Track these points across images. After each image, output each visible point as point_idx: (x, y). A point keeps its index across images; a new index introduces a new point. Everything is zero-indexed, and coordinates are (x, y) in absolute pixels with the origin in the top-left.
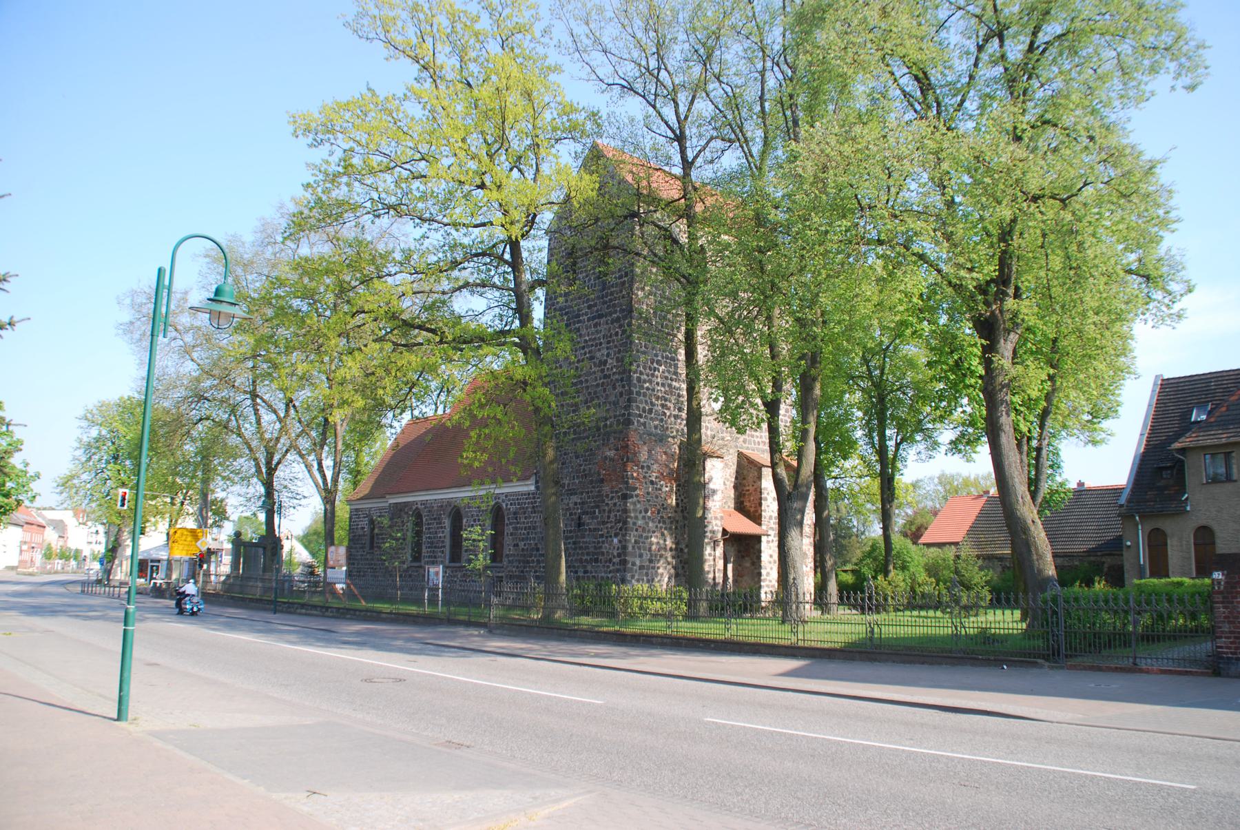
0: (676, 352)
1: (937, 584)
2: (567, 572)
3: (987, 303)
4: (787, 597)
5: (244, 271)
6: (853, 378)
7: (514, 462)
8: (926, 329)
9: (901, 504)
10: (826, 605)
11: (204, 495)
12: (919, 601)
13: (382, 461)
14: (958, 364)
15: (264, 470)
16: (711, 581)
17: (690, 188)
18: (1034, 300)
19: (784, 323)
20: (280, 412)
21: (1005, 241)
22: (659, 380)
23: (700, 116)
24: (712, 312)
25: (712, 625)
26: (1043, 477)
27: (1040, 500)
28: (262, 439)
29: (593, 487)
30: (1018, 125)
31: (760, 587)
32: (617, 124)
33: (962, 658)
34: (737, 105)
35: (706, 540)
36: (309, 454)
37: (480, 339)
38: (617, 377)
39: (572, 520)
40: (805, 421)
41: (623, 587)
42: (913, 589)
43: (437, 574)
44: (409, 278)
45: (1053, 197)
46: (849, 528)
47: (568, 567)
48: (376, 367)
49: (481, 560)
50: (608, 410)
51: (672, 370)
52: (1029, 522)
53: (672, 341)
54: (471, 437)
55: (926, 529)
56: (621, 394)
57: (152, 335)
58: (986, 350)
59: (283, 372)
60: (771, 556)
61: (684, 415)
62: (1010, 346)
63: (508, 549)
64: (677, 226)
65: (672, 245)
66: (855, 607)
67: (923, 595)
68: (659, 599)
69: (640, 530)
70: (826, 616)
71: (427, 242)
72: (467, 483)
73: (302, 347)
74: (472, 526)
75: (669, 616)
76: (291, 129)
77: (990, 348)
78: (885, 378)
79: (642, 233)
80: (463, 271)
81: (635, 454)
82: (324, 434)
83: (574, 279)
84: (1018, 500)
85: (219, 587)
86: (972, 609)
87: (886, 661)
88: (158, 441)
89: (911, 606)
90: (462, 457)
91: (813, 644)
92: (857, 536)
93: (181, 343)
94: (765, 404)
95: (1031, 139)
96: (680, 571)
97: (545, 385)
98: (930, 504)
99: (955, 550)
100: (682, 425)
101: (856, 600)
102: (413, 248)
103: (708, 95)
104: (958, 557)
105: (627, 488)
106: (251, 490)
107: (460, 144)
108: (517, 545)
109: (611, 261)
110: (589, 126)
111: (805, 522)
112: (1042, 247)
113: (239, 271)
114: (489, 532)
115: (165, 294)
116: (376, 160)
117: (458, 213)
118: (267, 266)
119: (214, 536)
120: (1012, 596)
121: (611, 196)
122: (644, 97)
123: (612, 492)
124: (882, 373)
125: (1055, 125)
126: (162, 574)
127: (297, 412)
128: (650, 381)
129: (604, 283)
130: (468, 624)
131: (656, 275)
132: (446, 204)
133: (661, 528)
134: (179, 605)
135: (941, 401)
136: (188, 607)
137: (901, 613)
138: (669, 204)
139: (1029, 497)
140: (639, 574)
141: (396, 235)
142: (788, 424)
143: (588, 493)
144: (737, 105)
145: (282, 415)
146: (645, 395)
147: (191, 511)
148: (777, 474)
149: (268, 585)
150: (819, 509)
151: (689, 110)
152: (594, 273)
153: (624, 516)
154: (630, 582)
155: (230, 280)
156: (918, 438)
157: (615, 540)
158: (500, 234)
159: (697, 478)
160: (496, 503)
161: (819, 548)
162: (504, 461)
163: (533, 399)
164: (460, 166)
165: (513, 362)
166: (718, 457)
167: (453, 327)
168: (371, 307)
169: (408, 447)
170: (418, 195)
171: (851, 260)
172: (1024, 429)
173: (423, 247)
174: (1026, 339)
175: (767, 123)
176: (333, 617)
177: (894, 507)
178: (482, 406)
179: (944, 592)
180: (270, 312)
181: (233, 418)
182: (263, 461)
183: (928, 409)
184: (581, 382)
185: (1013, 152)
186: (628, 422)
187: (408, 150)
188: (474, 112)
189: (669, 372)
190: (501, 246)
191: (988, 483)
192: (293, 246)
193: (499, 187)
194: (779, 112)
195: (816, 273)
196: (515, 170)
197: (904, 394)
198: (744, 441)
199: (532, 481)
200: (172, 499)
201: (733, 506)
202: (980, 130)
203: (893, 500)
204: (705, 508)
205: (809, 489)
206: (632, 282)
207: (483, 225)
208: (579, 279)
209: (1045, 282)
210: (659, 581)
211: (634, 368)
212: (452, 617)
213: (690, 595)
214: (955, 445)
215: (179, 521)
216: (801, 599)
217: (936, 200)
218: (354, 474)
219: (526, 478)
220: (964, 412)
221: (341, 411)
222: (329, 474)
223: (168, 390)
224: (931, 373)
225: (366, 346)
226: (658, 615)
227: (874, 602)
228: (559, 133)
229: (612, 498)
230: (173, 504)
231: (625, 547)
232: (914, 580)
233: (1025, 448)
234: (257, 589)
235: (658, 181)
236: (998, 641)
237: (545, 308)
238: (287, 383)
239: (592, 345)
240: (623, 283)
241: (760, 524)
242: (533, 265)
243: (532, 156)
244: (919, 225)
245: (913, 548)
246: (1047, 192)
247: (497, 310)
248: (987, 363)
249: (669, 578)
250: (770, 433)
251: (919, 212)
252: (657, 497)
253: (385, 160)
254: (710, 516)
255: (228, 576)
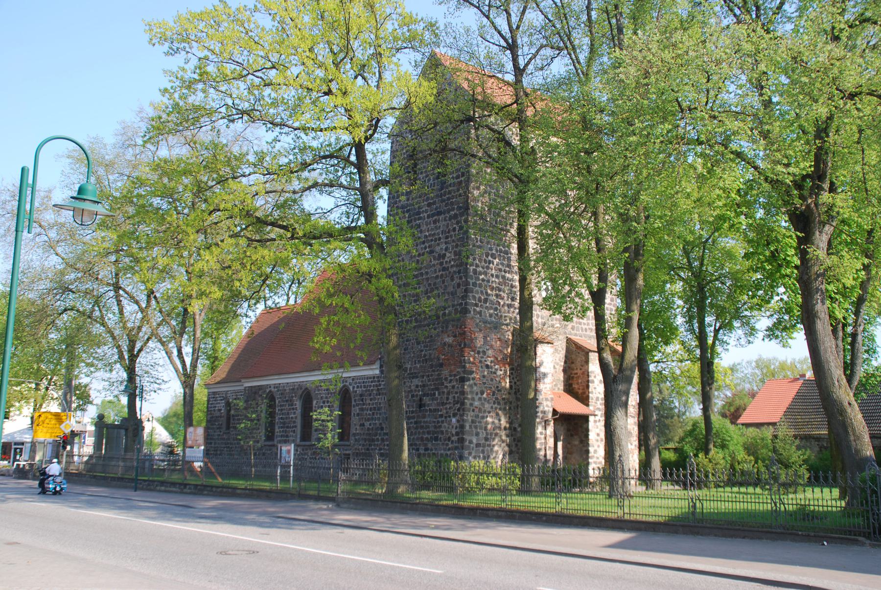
0: (509, 246)
1: (756, 462)
2: (409, 450)
3: (802, 197)
6: (673, 269)
7: (361, 348)
9: (720, 386)
10: (650, 480)
11: (69, 384)
12: (738, 478)
13: (238, 348)
14: (774, 256)
16: (542, 458)
17: (522, 93)
18: (849, 193)
19: (608, 219)
20: (141, 303)
21: (821, 138)
22: (493, 271)
23: (531, 26)
24: (541, 209)
25: (543, 499)
26: (859, 361)
27: (856, 383)
28: (124, 327)
29: (434, 371)
30: (836, 25)
31: (588, 464)
32: (453, 34)
33: (782, 533)
34: (565, 15)
35: (538, 420)
36: (169, 342)
37: (329, 234)
38: (455, 269)
39: (414, 401)
40: (629, 309)
42: (732, 467)
43: (288, 452)
45: (871, 93)
46: (672, 409)
47: (410, 445)
48: (232, 261)
49: (330, 439)
50: (446, 300)
51: (506, 262)
52: (846, 404)
53: (505, 235)
54: (321, 324)
55: (745, 410)
56: (459, 285)
57: (17, 231)
60: (598, 435)
62: (825, 238)
63: (355, 428)
64: (510, 129)
65: (505, 147)
66: (677, 483)
67: (743, 472)
68: (494, 475)
69: (477, 410)
70: (650, 491)
71: (278, 146)
73: (163, 243)
74: (322, 407)
75: (504, 491)
76: (147, 37)
77: (805, 241)
78: (704, 268)
79: (477, 137)
80: (312, 172)
81: (472, 340)
82: (183, 322)
83: (415, 179)
84: (834, 384)
85: (82, 467)
87: (708, 534)
88: (23, 331)
89: (731, 483)
90: (313, 342)
91: (639, 518)
92: (679, 417)
93: (46, 238)
94: (592, 293)
95: (849, 38)
96: (514, 449)
97: (389, 277)
98: (747, 386)
100: (515, 314)
101: (678, 476)
102: (265, 151)
103: (538, 6)
104: (776, 437)
105: (464, 372)
107: (308, 53)
108: (363, 425)
110: (427, 35)
111: (630, 403)
112: (858, 143)
113: (101, 172)
114: (336, 413)
115: (29, 192)
116: (229, 68)
117: (306, 118)
119: (77, 419)
120: (830, 475)
122: (478, 8)
123: (451, 376)
124: (702, 264)
125: (875, 23)
126: (25, 456)
127: (158, 302)
128: (486, 274)
130: (318, 498)
133: (496, 408)
134: (42, 485)
135: (758, 290)
136: (51, 486)
137: (722, 489)
138: (502, 109)
139: (845, 380)
140: (476, 451)
141: (250, 138)
142: (613, 312)
144: (565, 15)
145: (144, 306)
146: (480, 286)
147: (56, 396)
149: (128, 464)
151: (521, 20)
153: (462, 397)
154: (467, 459)
155: (93, 179)
157: (454, 420)
158: (346, 138)
159: (529, 363)
160: (344, 386)
161: (643, 428)
162: (352, 346)
164: (308, 74)
165: (360, 256)
166: (548, 343)
167: (303, 223)
169: (261, 334)
171: (672, 158)
172: (839, 315)
173: (274, 150)
174: (841, 231)
175: (594, 31)
176: (190, 493)
177: (713, 389)
179: (763, 469)
180: (131, 210)
181: (97, 309)
184: (422, 274)
185: (830, 52)
186: (465, 311)
187: (260, 58)
188: (320, 22)
189: (502, 264)
190: (348, 149)
191: (805, 367)
192: (153, 148)
193: (345, 93)
194: (604, 21)
195: (638, 173)
196: (360, 78)
197: (722, 283)
198: (573, 328)
199: (377, 365)
200: (37, 385)
201: (562, 388)
202: (798, 31)
203: (712, 383)
204: (536, 391)
205: (633, 372)
206: (468, 181)
208: (419, 179)
209: (861, 175)
210: (494, 458)
211: (470, 260)
212: (303, 492)
213: (523, 471)
215: (44, 405)
216: (627, 475)
217: (754, 101)
218: (212, 360)
219: (372, 363)
220: (782, 300)
221: (200, 302)
222: (188, 360)
223: (33, 282)
224: (748, 264)
227: (696, 478)
228: (400, 42)
229: (451, 380)
230: (37, 389)
231: (462, 427)
232: (733, 458)
233: (841, 334)
234: (119, 468)
236: (817, 518)
237: (388, 206)
239: (432, 240)
241: (587, 405)
242: (378, 167)
243: (375, 65)
244: (733, 125)
245: (732, 427)
246: (864, 89)
247: (344, 208)
248: (803, 254)
250: (596, 320)
251: (737, 113)
252: (492, 380)
253: (238, 68)
254: (541, 397)
255: (91, 457)
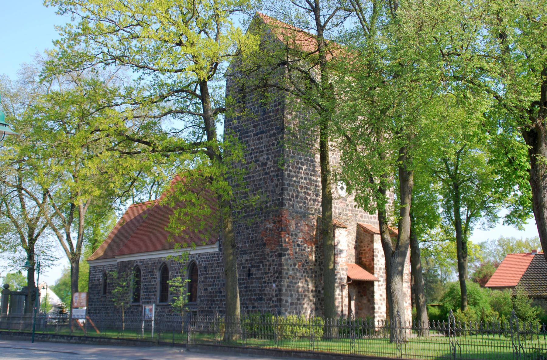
0: (314, 156)
1: (500, 316)
2: (241, 308)
4: (393, 324)
5: (11, 101)
7: (204, 232)
8: (489, 138)
9: (472, 259)
13: (112, 233)
15: (27, 241)
16: (340, 313)
17: (323, 44)
22: (303, 175)
25: (341, 344)
28: (26, 218)
29: (259, 249)
31: (374, 317)
35: (336, 285)
36: (60, 229)
37: (181, 149)
38: (274, 173)
39: (244, 271)
40: (403, 203)
41: (279, 318)
42: (482, 319)
44: (131, 107)
46: (435, 276)
47: (242, 304)
49: (181, 301)
50: (268, 196)
53: (311, 149)
55: (491, 276)
56: (277, 185)
58: (530, 152)
59: (42, 172)
60: (381, 295)
61: (320, 199)
65: (310, 84)
66: (441, 331)
67: (490, 324)
68: (304, 326)
69: (291, 278)
70: (421, 338)
72: (170, 247)
73: (55, 155)
74: (176, 276)
75: (311, 338)
77: (535, 150)
78: (458, 172)
79: (290, 76)
81: (287, 226)
83: (244, 108)
86: (527, 335)
89: (481, 331)
92: (441, 281)
96: (319, 306)
97: (225, 180)
98: (492, 259)
99: (513, 292)
100: (318, 206)
101: (442, 326)
102: (133, 86)
104: (515, 297)
105: (282, 249)
106: (17, 255)
107: (164, 14)
109: (269, 95)
111: (404, 272)
114: (187, 280)
117: (163, 62)
118: (28, 98)
121: (268, 50)
123: (271, 252)
124: (457, 169)
127: (52, 199)
128: (297, 177)
129: (264, 110)
130: (173, 345)
131: (299, 104)
132: (155, 57)
135: (498, 187)
137: (475, 336)
140: (291, 308)
141: (121, 77)
142: (391, 205)
143: (255, 253)
145: (41, 202)
146: (293, 186)
148: (385, 239)
150: (414, 263)
152: (257, 103)
153: (280, 268)
154: (284, 314)
156: (483, 213)
157: (274, 285)
158: (193, 77)
159: (329, 242)
160: (192, 261)
161: (415, 290)
162: (196, 231)
163: (217, 189)
164: (164, 29)
165: (203, 164)
166: (343, 227)
167: (162, 140)
168: (106, 127)
169: (131, 223)
170: (136, 50)
177: (467, 261)
178: (183, 194)
179: (506, 321)
182: (27, 234)
183: (489, 193)
184: (250, 177)
186: (282, 204)
187: (128, 18)
189: (309, 170)
190: (194, 86)
191: (536, 244)
192: (47, 84)
193: (192, 44)
196: (203, 32)
197: (472, 182)
199: (217, 245)
201: (354, 261)
203: (466, 256)
204: (335, 263)
205: (407, 249)
206: (283, 109)
207: (180, 70)
208: (247, 107)
210: (304, 313)
213: (326, 323)
214: (509, 219)
216: (403, 325)
219: (213, 243)
220: (516, 195)
222: (75, 243)
224: (492, 168)
225: (101, 153)
226: (304, 337)
227: (455, 328)
228: (232, 6)
229: (272, 256)
231: (280, 290)
232: (483, 313)
235: (300, 39)
237: (225, 127)
238: (45, 179)
239: (257, 152)
240: (278, 110)
241: (373, 273)
243: (215, 23)
245: (481, 290)
247: (191, 129)
248: (533, 161)
249: (311, 311)
252: (302, 255)
253: (111, 25)
254: (338, 267)
